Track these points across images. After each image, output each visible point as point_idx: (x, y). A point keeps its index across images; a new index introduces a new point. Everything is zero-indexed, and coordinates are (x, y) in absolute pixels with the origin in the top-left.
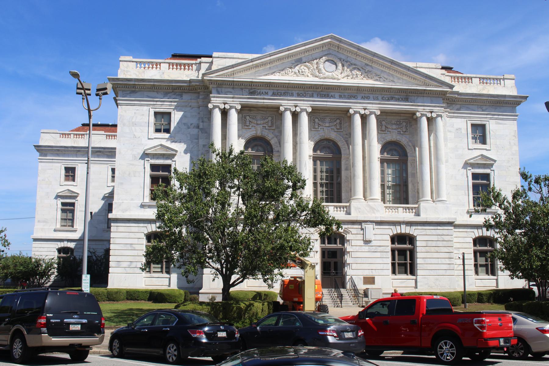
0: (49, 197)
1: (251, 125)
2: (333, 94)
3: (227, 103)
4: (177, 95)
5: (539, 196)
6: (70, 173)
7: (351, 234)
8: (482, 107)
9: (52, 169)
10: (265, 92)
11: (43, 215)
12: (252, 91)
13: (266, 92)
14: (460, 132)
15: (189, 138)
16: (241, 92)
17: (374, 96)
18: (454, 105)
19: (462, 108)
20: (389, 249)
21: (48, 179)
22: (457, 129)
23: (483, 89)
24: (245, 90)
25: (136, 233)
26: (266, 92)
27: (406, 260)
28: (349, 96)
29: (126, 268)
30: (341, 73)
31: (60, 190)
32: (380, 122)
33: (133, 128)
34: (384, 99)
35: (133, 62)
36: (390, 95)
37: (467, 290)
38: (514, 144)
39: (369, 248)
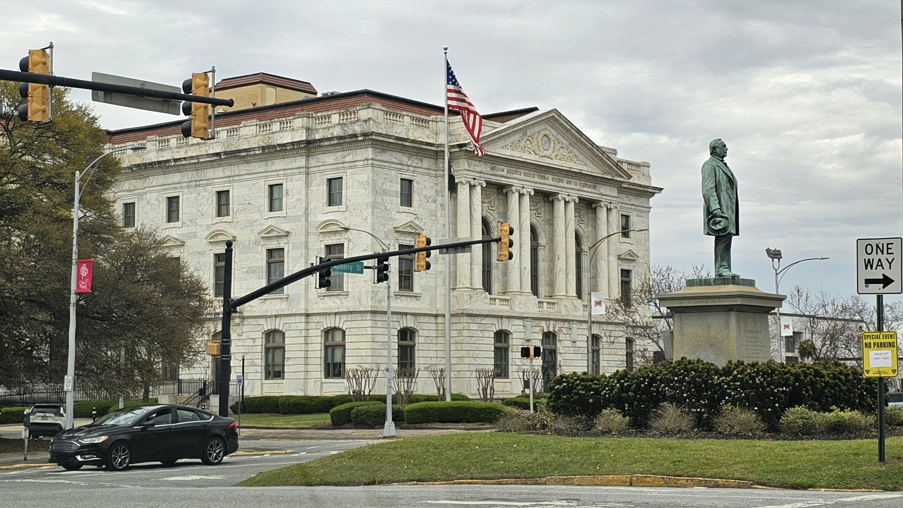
33: (384, 197)
35: (382, 110)
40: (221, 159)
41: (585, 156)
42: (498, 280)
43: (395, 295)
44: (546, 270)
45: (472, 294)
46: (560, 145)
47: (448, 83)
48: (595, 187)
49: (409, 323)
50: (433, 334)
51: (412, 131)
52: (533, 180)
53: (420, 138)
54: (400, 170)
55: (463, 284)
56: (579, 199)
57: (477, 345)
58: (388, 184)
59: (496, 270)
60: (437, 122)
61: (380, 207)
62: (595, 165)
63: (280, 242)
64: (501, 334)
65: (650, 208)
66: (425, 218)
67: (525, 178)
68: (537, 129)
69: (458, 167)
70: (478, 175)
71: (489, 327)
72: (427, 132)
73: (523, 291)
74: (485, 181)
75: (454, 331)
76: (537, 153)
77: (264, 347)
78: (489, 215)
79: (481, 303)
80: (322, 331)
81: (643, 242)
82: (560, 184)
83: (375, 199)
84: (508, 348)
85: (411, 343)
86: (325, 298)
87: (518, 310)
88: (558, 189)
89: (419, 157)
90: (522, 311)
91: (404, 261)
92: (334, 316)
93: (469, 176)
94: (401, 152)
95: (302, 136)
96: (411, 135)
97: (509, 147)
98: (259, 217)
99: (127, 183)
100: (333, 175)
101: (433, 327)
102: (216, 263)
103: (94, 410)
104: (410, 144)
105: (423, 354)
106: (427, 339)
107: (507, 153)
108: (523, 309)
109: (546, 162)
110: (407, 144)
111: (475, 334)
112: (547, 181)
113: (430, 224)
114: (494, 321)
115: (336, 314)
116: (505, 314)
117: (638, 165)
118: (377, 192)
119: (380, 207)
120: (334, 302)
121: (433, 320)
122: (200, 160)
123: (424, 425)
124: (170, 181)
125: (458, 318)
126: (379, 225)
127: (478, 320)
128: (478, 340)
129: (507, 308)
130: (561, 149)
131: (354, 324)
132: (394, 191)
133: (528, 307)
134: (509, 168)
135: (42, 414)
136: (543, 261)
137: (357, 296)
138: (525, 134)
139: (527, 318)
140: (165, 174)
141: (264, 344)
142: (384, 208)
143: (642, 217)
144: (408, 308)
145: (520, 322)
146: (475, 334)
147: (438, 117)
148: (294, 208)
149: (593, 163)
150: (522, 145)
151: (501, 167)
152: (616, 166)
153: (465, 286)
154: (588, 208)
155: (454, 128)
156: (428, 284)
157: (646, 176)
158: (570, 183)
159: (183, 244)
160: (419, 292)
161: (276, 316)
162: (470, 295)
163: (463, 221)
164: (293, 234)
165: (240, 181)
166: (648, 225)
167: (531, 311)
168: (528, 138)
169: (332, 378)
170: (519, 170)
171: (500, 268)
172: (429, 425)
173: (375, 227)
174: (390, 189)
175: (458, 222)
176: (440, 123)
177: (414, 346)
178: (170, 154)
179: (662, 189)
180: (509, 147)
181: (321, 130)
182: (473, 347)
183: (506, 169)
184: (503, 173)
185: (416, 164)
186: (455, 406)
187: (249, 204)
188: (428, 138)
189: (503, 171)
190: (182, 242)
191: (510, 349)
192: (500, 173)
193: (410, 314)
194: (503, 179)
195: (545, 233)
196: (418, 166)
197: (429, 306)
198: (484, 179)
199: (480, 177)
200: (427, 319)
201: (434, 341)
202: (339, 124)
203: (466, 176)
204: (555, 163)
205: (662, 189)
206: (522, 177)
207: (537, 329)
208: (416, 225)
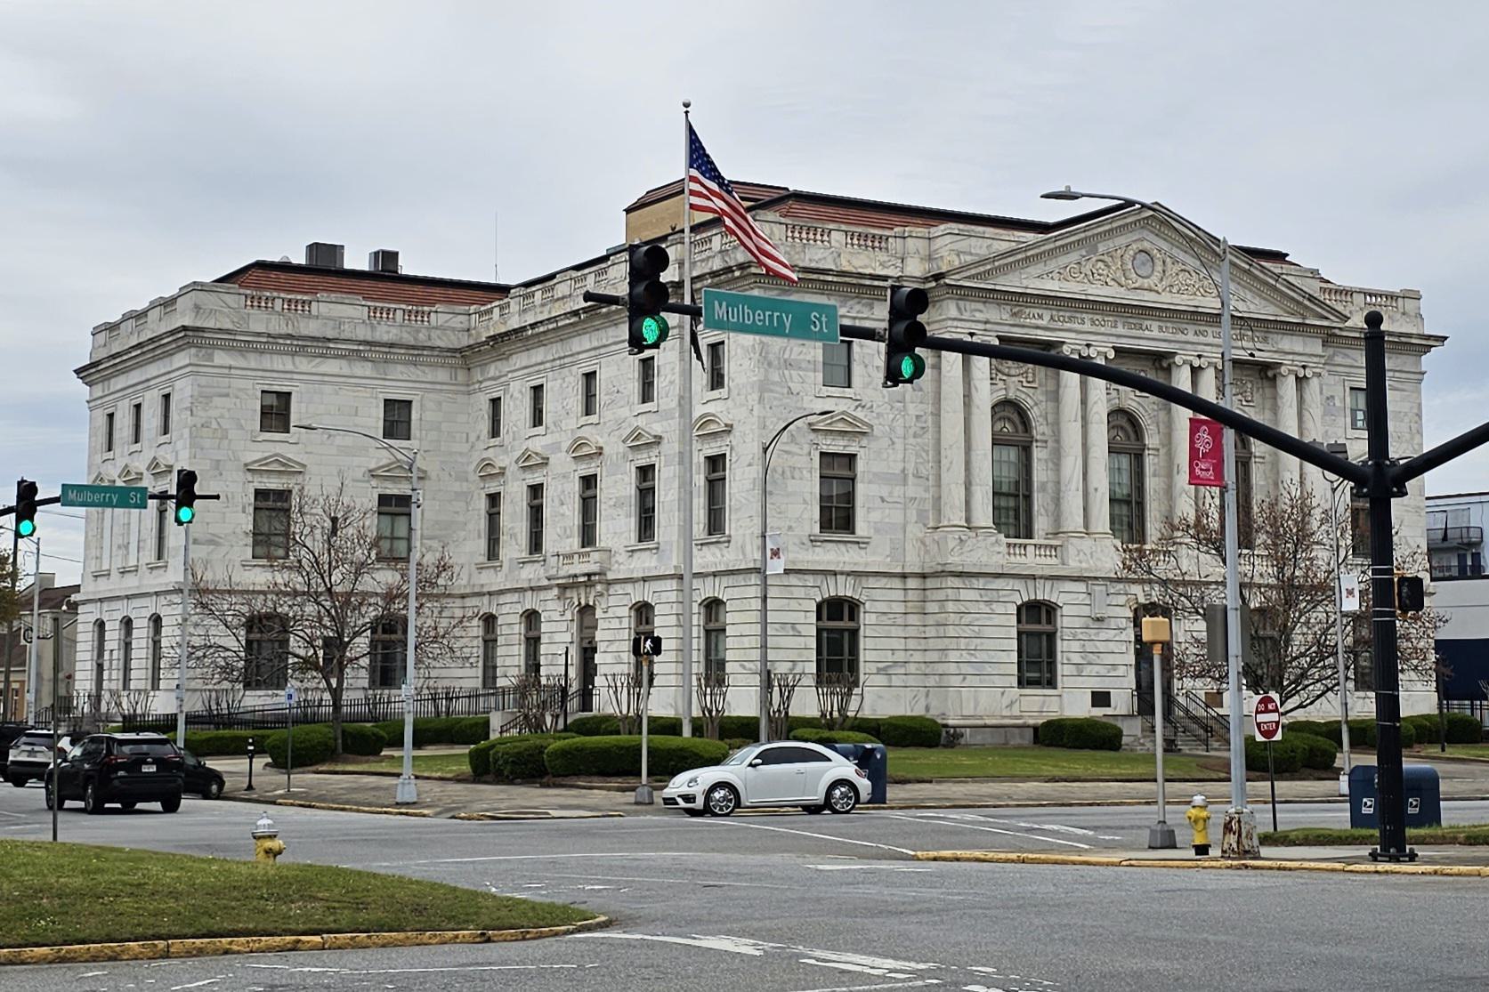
0: (221, 474)
4: (863, 305)
5: (901, 466)
6: (276, 413)
9: (227, 395)
11: (208, 524)
15: (886, 400)
17: (1215, 329)
21: (218, 423)
22: (1328, 398)
25: (801, 601)
27: (649, 741)
29: (961, 665)
30: (1162, 280)
33: (786, 372)
35: (781, 224)
37: (1269, 783)
40: (581, 321)
41: (1239, 284)
42: (1046, 511)
43: (812, 541)
44: (1161, 493)
45: (963, 537)
46: (1180, 267)
47: (691, 166)
48: (1265, 340)
49: (844, 589)
50: (900, 608)
51: (848, 257)
52: (1113, 331)
53: (866, 267)
55: (949, 520)
56: (1116, 351)
57: (976, 628)
58: (795, 349)
59: (1040, 495)
60: (904, 238)
61: (778, 389)
62: (1265, 299)
63: (651, 454)
64: (1040, 608)
65: (1424, 373)
66: (879, 406)
67: (1094, 329)
68: (1122, 240)
69: (940, 315)
70: (981, 326)
71: (1004, 596)
72: (882, 256)
73: (1090, 531)
75: (934, 604)
76: (1123, 283)
77: (522, 637)
78: (1023, 396)
79: (992, 551)
80: (700, 604)
81: (1408, 436)
82: (1180, 337)
83: (766, 376)
84: (1055, 633)
86: (704, 547)
87: (1074, 565)
88: (1172, 345)
89: (864, 301)
90: (1084, 565)
91: (835, 481)
93: (959, 330)
94: (823, 294)
95: (674, 275)
96: (844, 263)
97: (1055, 275)
98: (628, 414)
99: (493, 367)
100: (713, 338)
101: (899, 595)
102: (583, 492)
103: (251, 744)
104: (835, 279)
105: (876, 645)
106: (884, 618)
107: (1052, 286)
108: (1087, 562)
109: (1148, 298)
110: (830, 278)
111: (972, 608)
112: (1146, 332)
113: (891, 416)
114: (1018, 584)
116: (1040, 573)
117: (1392, 297)
118: (770, 364)
119: (778, 389)
120: (714, 554)
121: (897, 583)
122: (560, 324)
123: (567, 781)
124: (533, 361)
125: (939, 579)
126: (775, 420)
127: (980, 583)
128: (978, 619)
129: (1054, 561)
130: (1181, 275)
131: (735, 593)
132: (809, 361)
133: (1098, 559)
134: (1054, 313)
135: (29, 748)
136: (1155, 475)
137: (740, 544)
138: (1094, 250)
139: (1096, 578)
140: (528, 350)
141: (632, 626)
142: (785, 390)
143: (1403, 390)
144: (839, 562)
145: (1081, 587)
146: (972, 608)
147: (907, 229)
148: (667, 396)
149: (1260, 296)
150: (1087, 269)
151: (1036, 311)
152: (1309, 300)
153: (952, 523)
154: (1262, 379)
155: (936, 247)
156: (887, 520)
157: (1409, 316)
158: (1203, 334)
159: (545, 462)
160: (865, 534)
161: (644, 579)
162: (960, 538)
163: (948, 409)
164: (666, 441)
165: (608, 354)
166: (1420, 405)
168: (1102, 257)
170: (1078, 315)
171: (1050, 491)
173: (767, 424)
174: (802, 357)
175: (942, 412)
176: (909, 239)
177: (854, 633)
178: (532, 317)
179: (1446, 338)
180: (1055, 275)
181: (699, 264)
182: (968, 632)
183: (1047, 315)
184: (1040, 322)
185: (858, 312)
186: (627, 745)
187: (618, 392)
188: (884, 267)
189: (1041, 317)
190: (543, 458)
191: (1059, 634)
192: (1033, 321)
193: (842, 573)
194: (1039, 332)
195: (1158, 426)
196: (860, 315)
197: (889, 559)
198: (996, 334)
199: (985, 330)
200: (883, 582)
201: (900, 621)
202: (721, 252)
203: (953, 330)
204: (1166, 299)
205: (1446, 338)
206: (1087, 327)
207: (1122, 600)
208: (855, 418)
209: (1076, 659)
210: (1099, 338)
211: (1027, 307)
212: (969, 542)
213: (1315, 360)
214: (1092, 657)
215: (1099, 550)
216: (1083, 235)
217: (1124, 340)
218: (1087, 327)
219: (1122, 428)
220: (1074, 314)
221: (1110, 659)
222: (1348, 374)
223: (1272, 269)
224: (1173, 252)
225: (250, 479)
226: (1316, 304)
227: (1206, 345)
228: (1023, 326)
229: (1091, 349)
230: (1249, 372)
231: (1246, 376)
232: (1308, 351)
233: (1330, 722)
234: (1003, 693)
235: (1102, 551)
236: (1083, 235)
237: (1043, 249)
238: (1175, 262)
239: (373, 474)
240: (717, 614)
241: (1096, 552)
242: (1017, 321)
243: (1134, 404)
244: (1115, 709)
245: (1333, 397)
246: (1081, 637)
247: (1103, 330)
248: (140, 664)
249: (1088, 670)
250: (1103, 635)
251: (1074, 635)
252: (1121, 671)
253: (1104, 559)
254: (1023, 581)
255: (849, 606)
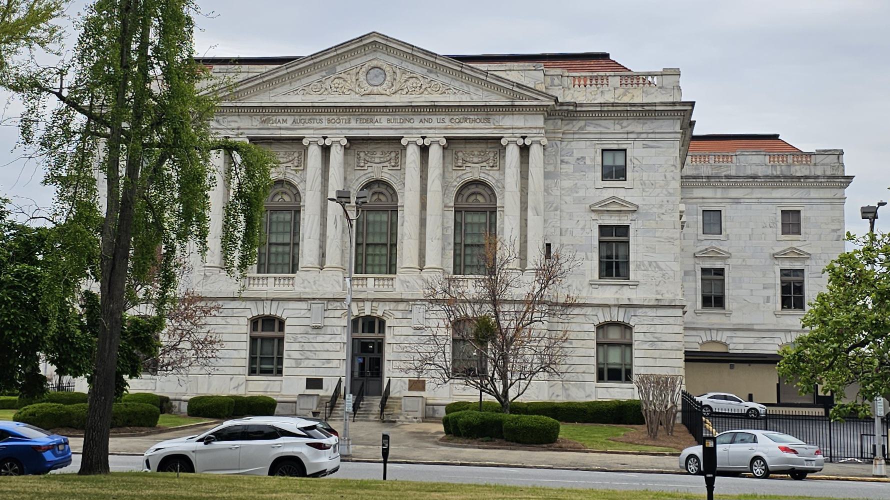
1: (366, 165)
2: (378, 117)
3: (426, 137)
7: (394, 318)
8: (621, 122)
10: (283, 120)
12: (264, 119)
13: (285, 119)
14: (583, 163)
16: (250, 121)
17: (439, 117)
18: (575, 122)
19: (588, 126)
20: (246, 338)
22: (578, 159)
23: (624, 94)
24: (255, 118)
26: (285, 119)
28: (402, 121)
31: (808, 262)
32: (455, 154)
34: (453, 121)
36: (461, 115)
38: (673, 178)
39: (419, 339)
45: (207, 274)
52: (347, 126)
54: (599, 139)
56: (348, 140)
64: (274, 320)
74: (248, 137)
82: (407, 125)
85: (279, 334)
88: (398, 131)
91: (614, 244)
92: (270, 302)
109: (368, 101)
115: (273, 300)
134: (297, 117)
145: (304, 305)
151: (281, 118)
167: (328, 290)
169: (258, 375)
170: (317, 117)
172: (541, 445)
177: (281, 340)
183: (290, 120)
184: (284, 125)
189: (285, 121)
192: (279, 125)
194: (282, 132)
198: (344, 135)
209: (296, 355)
210: (334, 131)
211: (273, 116)
212: (212, 277)
213: (535, 131)
214: (309, 354)
215: (321, 279)
216: (311, 62)
217: (355, 132)
218: (325, 124)
219: (473, 194)
220: (314, 117)
221: (326, 355)
222: (599, 139)
223: (480, 68)
224: (403, 65)
225: (698, 262)
226: (525, 90)
227: (429, 129)
228: (269, 129)
229: (426, 140)
230: (493, 145)
231: (491, 148)
232: (528, 125)
233: (460, 402)
234: (231, 379)
235: (324, 280)
236: (311, 62)
237: (277, 75)
238: (404, 72)
239: (775, 257)
240: (607, 334)
241: (318, 281)
242: (266, 126)
243: (387, 176)
244: (327, 390)
245: (583, 158)
246: (301, 340)
247: (338, 126)
248: (679, 371)
249: (305, 363)
250: (320, 339)
251: (295, 339)
252: (335, 364)
253: (325, 285)
254: (254, 302)
255: (280, 322)
